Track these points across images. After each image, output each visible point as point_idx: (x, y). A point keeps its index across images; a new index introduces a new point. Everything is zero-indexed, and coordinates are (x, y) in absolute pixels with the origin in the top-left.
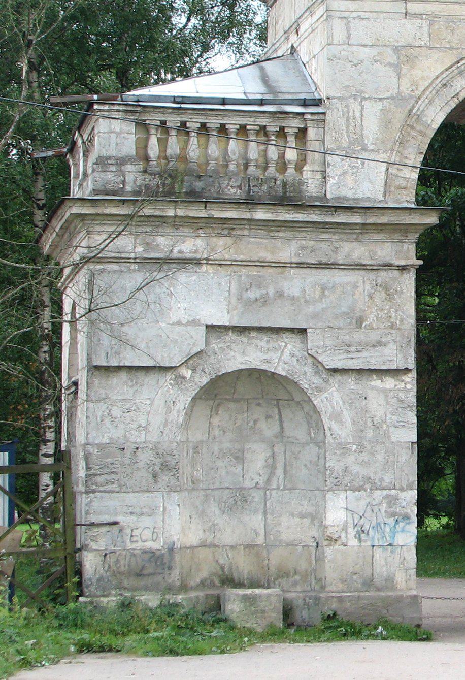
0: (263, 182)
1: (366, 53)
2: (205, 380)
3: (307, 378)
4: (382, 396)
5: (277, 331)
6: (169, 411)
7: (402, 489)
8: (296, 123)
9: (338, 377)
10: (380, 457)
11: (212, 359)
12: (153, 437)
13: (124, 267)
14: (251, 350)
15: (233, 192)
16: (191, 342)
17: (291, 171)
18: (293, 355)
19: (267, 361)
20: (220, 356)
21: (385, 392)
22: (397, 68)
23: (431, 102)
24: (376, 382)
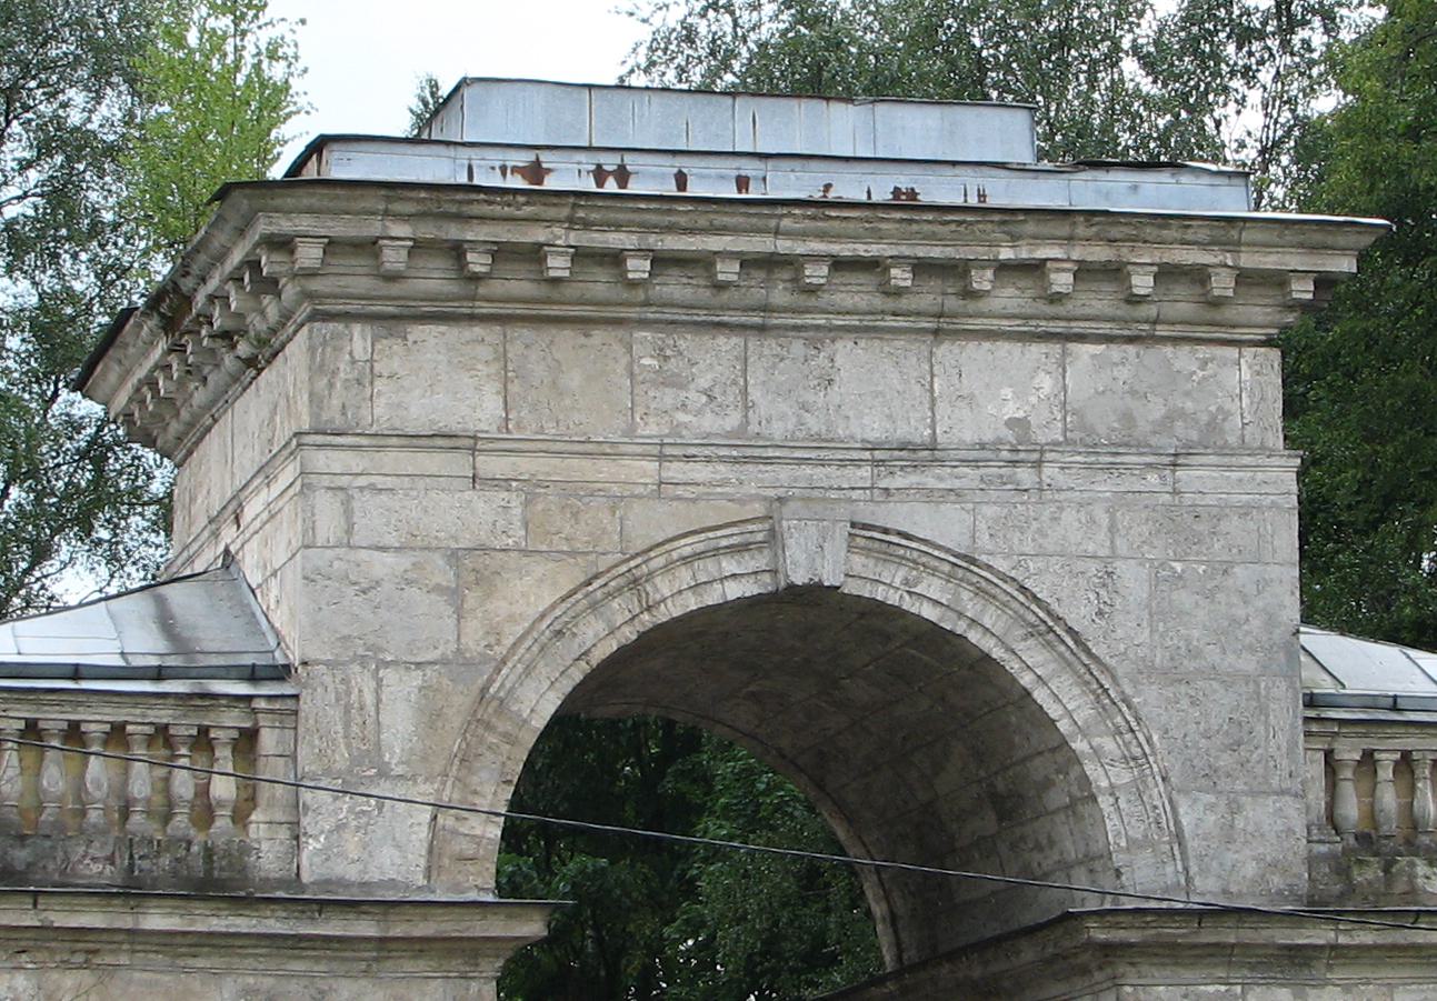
1: (384, 565)
8: (233, 719)
22: (455, 596)
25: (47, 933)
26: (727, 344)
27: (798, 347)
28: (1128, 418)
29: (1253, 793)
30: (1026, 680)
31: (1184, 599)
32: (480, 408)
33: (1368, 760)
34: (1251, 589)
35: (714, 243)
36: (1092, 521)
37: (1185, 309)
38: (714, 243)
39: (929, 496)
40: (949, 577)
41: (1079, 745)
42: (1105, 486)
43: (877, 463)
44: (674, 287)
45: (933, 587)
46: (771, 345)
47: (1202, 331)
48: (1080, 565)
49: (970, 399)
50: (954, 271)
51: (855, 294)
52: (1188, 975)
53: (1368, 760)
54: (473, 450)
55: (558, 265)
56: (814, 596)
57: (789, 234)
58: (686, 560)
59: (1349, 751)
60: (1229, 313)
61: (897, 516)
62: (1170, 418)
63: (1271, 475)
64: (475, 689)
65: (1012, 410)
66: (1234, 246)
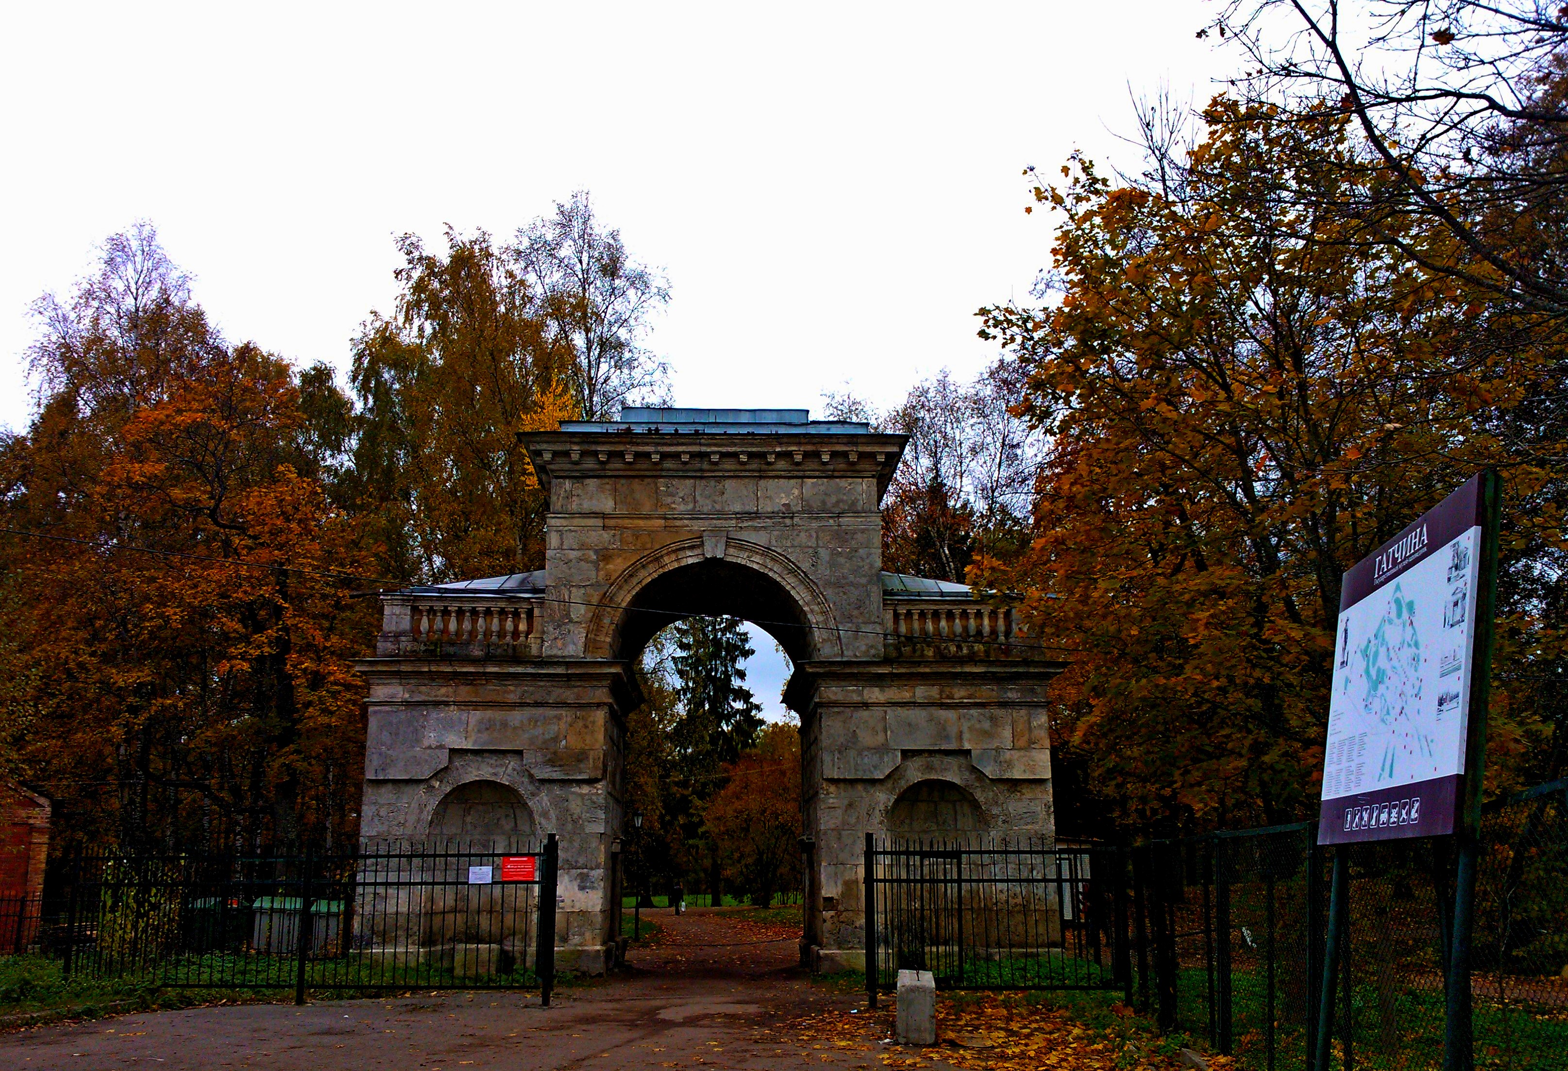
0: (498, 646)
1: (573, 555)
2: (449, 789)
3: (524, 788)
4: (580, 799)
5: (504, 753)
6: (421, 812)
7: (592, 869)
8: (525, 606)
9: (547, 786)
10: (576, 845)
11: (455, 774)
12: (409, 831)
13: (394, 708)
14: (483, 766)
15: (477, 652)
16: (438, 761)
17: (522, 639)
18: (514, 770)
19: (495, 774)
20: (461, 771)
21: (582, 796)
22: (596, 564)
23: (621, 588)
24: (576, 789)
25: (456, 674)
26: (689, 482)
27: (712, 483)
28: (824, 503)
29: (864, 623)
30: (788, 588)
31: (842, 560)
32: (607, 504)
33: (909, 614)
34: (865, 556)
35: (680, 449)
36: (811, 536)
37: (843, 466)
38: (680, 449)
39: (756, 529)
40: (762, 555)
41: (806, 609)
42: (815, 525)
43: (737, 519)
44: (668, 464)
45: (757, 558)
46: (704, 482)
47: (849, 474)
48: (806, 550)
49: (770, 498)
50: (762, 456)
51: (729, 465)
52: (843, 683)
53: (909, 614)
54: (604, 518)
55: (629, 458)
56: (713, 563)
57: (704, 445)
58: (674, 551)
59: (902, 610)
60: (858, 467)
61: (744, 535)
62: (838, 502)
63: (872, 519)
64: (602, 592)
65: (784, 501)
66: (856, 444)
